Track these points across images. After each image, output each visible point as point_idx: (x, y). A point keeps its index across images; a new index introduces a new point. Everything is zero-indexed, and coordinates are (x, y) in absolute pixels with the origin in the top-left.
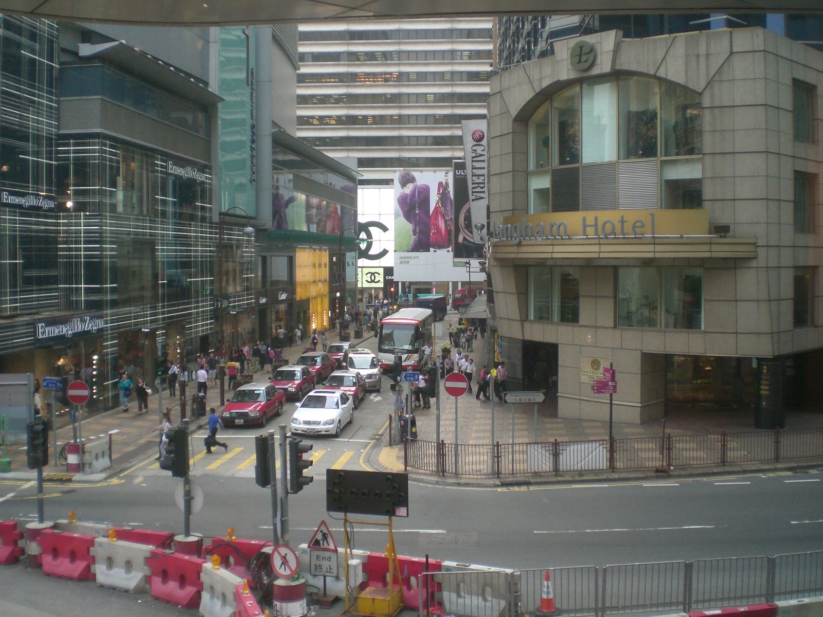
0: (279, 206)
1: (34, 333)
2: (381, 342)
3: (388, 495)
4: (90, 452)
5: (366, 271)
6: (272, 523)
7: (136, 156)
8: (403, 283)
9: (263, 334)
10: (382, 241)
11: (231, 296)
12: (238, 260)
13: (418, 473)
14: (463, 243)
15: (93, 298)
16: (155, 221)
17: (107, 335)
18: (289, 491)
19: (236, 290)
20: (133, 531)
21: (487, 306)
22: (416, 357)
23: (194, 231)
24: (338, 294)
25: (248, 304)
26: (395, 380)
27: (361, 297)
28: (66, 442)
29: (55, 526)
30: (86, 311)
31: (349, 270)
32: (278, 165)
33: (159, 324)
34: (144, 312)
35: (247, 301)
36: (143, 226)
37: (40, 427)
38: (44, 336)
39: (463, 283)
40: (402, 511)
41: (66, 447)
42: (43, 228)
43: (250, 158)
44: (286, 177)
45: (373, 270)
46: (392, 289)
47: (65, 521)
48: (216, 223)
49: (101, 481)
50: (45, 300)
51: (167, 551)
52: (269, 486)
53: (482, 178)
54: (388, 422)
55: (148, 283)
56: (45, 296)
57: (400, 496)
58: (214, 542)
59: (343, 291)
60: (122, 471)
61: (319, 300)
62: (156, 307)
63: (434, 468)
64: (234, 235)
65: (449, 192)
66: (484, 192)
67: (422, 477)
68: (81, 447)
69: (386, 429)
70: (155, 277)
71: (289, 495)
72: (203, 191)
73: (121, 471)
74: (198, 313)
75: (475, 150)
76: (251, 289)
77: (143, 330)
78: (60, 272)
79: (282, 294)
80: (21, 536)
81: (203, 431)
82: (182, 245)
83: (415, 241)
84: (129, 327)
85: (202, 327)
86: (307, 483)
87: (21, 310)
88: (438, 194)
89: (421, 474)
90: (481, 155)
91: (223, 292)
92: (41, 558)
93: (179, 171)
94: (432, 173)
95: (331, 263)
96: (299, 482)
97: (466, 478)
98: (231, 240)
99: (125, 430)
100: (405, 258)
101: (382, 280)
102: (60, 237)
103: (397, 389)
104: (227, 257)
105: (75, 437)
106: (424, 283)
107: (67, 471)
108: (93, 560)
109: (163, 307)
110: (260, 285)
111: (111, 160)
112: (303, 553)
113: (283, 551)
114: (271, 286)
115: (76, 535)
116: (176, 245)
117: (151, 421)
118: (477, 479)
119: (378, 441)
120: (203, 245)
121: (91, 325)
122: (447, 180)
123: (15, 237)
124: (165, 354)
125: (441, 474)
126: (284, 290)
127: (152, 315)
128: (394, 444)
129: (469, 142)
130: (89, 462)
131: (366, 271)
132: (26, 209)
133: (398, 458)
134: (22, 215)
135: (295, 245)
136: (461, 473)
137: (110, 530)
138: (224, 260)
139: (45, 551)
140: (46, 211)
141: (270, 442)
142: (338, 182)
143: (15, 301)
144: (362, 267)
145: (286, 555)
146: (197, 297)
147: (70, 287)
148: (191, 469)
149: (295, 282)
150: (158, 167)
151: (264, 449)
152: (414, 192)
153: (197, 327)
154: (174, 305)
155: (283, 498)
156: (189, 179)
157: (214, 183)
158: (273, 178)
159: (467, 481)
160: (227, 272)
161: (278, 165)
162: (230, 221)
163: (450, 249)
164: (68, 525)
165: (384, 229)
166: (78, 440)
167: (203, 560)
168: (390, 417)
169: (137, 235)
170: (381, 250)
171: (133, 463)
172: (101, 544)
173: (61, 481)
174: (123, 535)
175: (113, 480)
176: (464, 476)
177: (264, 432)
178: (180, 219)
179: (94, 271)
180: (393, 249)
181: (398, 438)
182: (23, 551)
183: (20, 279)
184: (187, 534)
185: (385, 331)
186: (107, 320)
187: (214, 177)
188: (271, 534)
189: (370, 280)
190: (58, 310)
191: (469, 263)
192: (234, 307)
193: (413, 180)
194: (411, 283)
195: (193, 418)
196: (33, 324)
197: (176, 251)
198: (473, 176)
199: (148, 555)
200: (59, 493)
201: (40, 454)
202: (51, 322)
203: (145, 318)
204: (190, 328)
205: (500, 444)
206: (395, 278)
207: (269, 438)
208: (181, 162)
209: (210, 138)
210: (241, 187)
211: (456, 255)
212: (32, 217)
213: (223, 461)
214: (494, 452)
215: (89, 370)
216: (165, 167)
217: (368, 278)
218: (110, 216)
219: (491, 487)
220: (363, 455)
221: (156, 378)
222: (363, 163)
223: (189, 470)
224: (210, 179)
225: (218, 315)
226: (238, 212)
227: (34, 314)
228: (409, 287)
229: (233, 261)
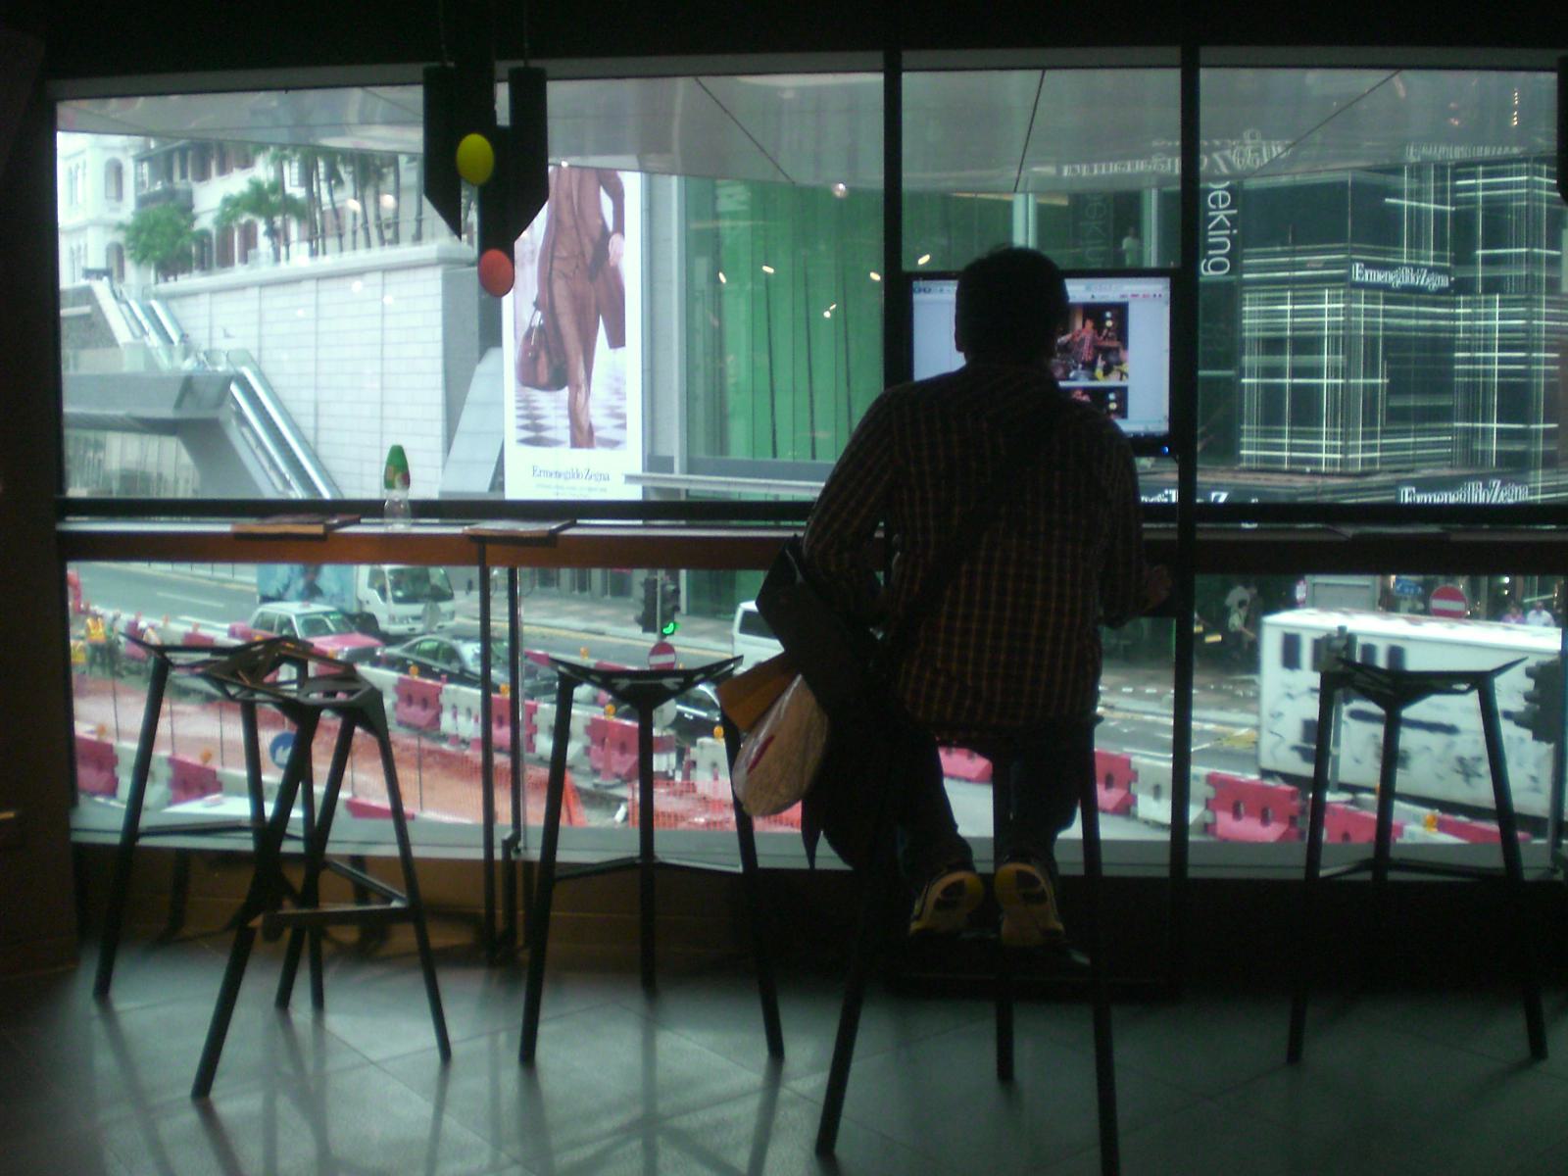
78: (1456, 401)
102: (1459, 339)
132: (1396, 291)
134: (1387, 301)
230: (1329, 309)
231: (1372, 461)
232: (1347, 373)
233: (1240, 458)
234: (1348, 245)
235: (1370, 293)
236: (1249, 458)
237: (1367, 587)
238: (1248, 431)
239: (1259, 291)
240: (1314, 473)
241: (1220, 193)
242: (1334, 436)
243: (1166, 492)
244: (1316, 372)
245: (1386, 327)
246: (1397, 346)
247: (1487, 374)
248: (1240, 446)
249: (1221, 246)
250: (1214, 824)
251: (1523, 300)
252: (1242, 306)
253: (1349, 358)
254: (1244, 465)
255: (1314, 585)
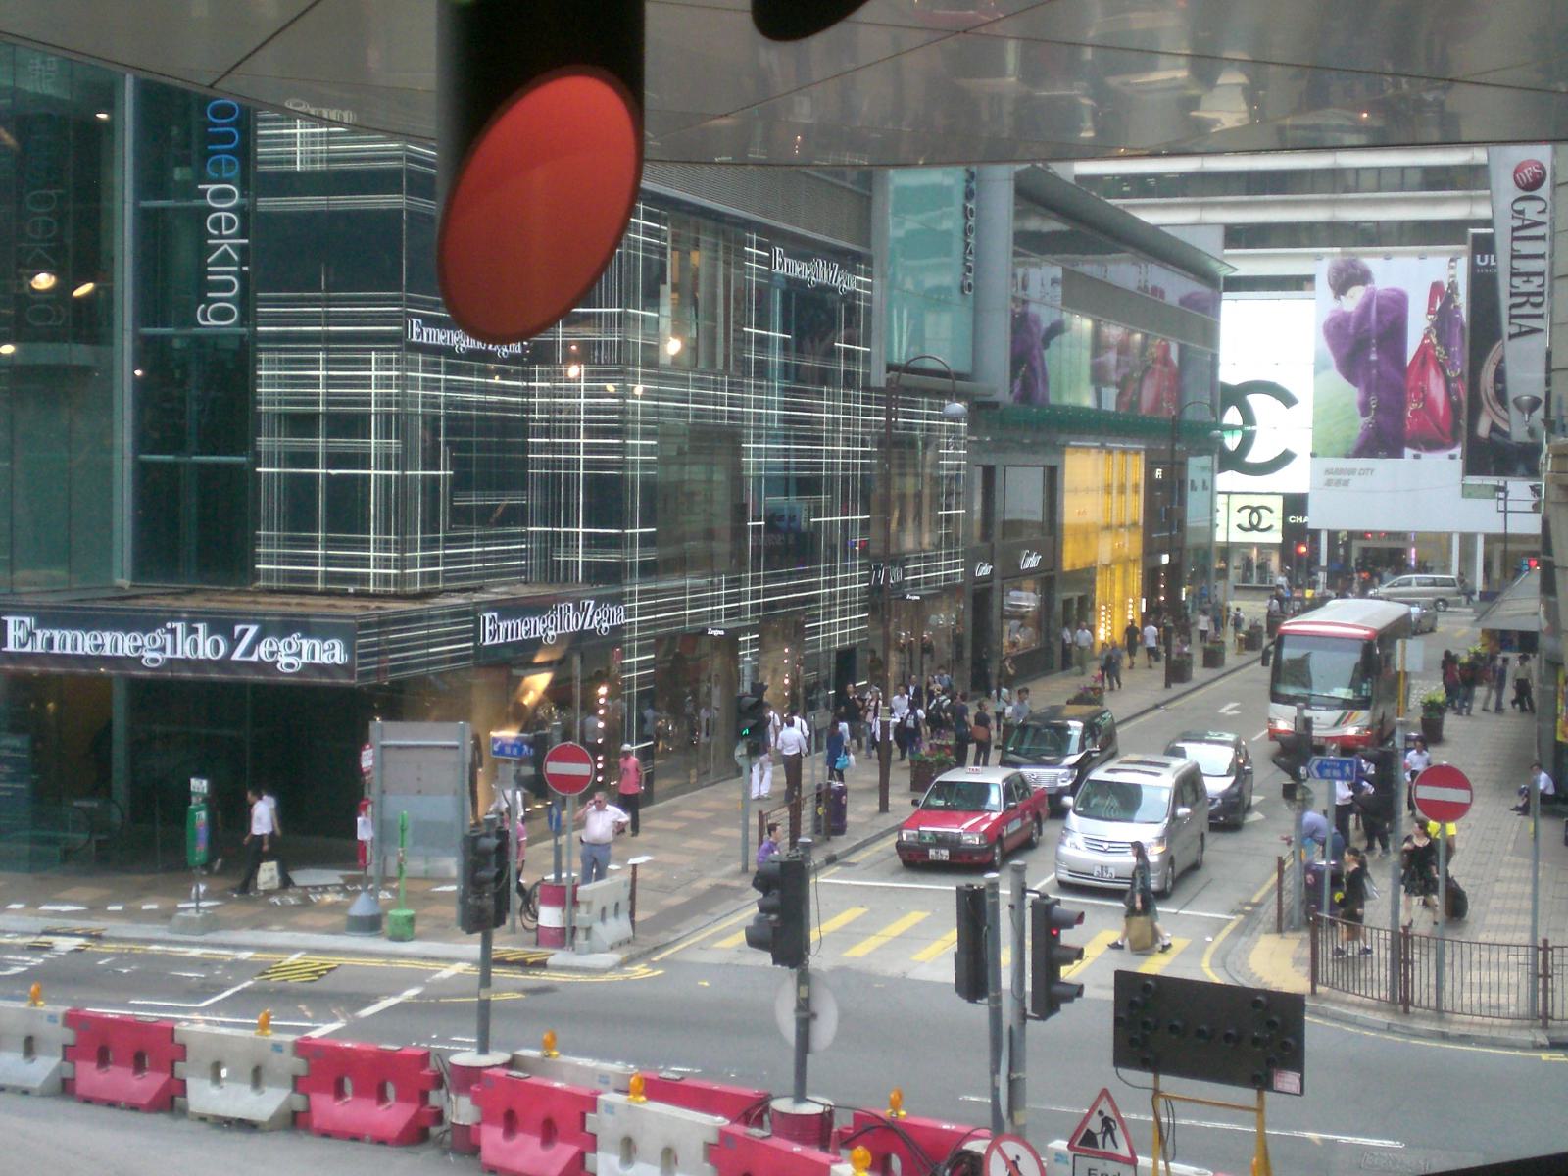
0: (1028, 346)
1: (475, 634)
2: (1277, 678)
3: (1256, 1041)
4: (589, 903)
5: (1238, 501)
6: (989, 1091)
7: (702, 238)
8: (1333, 535)
9: (971, 675)
10: (1276, 429)
11: (908, 559)
12: (928, 471)
13: (1342, 1002)
14: (1490, 438)
15: (599, 558)
16: (741, 385)
17: (631, 640)
18: (1029, 1012)
19: (921, 544)
20: (682, 1082)
21: (1542, 601)
22: (1363, 716)
23: (828, 408)
24: (1165, 559)
25: (947, 578)
26: (1295, 775)
27: (1223, 565)
28: (538, 878)
29: (510, 1064)
30: (587, 587)
31: (1194, 501)
32: (1029, 244)
33: (746, 620)
34: (714, 590)
35: (949, 570)
36: (716, 396)
37: (492, 842)
38: (495, 641)
39: (1489, 539)
40: (1288, 1080)
41: (538, 890)
42: (494, 398)
43: (961, 235)
44: (1044, 275)
45: (1255, 501)
46: (1303, 549)
47: (533, 1053)
48: (879, 390)
49: (611, 969)
50: (497, 560)
51: (755, 1132)
52: (985, 1000)
53: (1537, 281)
54: (1275, 876)
55: (723, 524)
56: (496, 552)
57: (1285, 1045)
58: (857, 1118)
59: (1176, 548)
60: (657, 949)
61: (1119, 572)
62: (739, 580)
63: (1382, 993)
64: (920, 416)
65: (1457, 307)
66: (1540, 316)
67: (1344, 1011)
68: (569, 891)
69: (1270, 892)
70: (740, 511)
71: (1028, 1021)
72: (852, 310)
73: (655, 948)
74: (832, 596)
75: (1521, 212)
76: (957, 544)
77: (710, 632)
78: (531, 499)
79: (1028, 555)
80: (438, 1082)
81: (838, 868)
82: (799, 439)
83: (1366, 430)
84: (678, 624)
85: (840, 628)
86: (1069, 998)
87: (447, 580)
88: (1429, 313)
89: (1352, 1004)
90: (1536, 224)
91: (893, 550)
92: (478, 1132)
93: (802, 270)
94: (1414, 260)
95: (1151, 484)
96: (1051, 995)
97: (1462, 1023)
98: (912, 429)
99: (667, 857)
100: (1340, 472)
101: (1278, 525)
102: (533, 420)
103: (1298, 796)
104: (901, 466)
105: (558, 870)
106: (1390, 535)
107: (537, 943)
108: (592, 1143)
109: (755, 581)
110: (977, 530)
111: (647, 247)
112: (1057, 1161)
113: (1012, 1148)
114: (1004, 535)
115: (557, 1085)
116: (787, 439)
117: (723, 838)
118: (1491, 1026)
119: (1249, 919)
120: (847, 439)
121: (599, 619)
122: (1453, 276)
123: (436, 418)
124: (758, 689)
125: (1401, 1008)
126: (1034, 547)
127: (730, 598)
128: (1288, 929)
129: (1505, 188)
130: (588, 925)
131: (1238, 501)
132: (459, 356)
133: (1297, 961)
134: (452, 369)
135: (1062, 439)
136: (1449, 1008)
137: (632, 1076)
138: (894, 471)
139: (487, 1117)
140: (504, 361)
141: (989, 900)
142: (1175, 287)
143: (433, 561)
144: (1229, 493)
145: (1018, 1157)
146: (832, 559)
147: (552, 532)
148: (813, 950)
149: (1062, 525)
150: (751, 261)
151: (975, 916)
152: (1366, 307)
153: (829, 628)
154: (779, 578)
155: (1015, 1028)
156: (823, 289)
157: (877, 294)
158: (1015, 276)
159: (1464, 1030)
160: (902, 497)
161: (1029, 244)
162: (915, 381)
163: (1458, 451)
164: (543, 1061)
165: (1288, 400)
166: (564, 875)
167: (832, 1157)
168: (1281, 862)
169: (701, 417)
170: (1277, 453)
171: (680, 935)
172: (611, 1108)
173: (522, 965)
174: (659, 1090)
175: (636, 968)
176: (1457, 1018)
177: (979, 882)
178: (798, 380)
179: (607, 498)
180: (1310, 450)
181: (1298, 914)
182: (439, 1117)
183: (444, 512)
184: (800, 1097)
185: (1288, 653)
186: (632, 608)
187: (877, 282)
188: (987, 1116)
189: (1247, 525)
190: (526, 583)
191: (1503, 489)
192: (916, 583)
193: (1364, 278)
194: (1352, 535)
195: (819, 837)
196: (472, 614)
197: (786, 453)
198: (1513, 275)
199: (714, 1138)
200: (519, 992)
201: (488, 902)
202: (510, 609)
203: (713, 603)
204: (815, 631)
205: (1550, 945)
206: (1312, 520)
207: (988, 891)
208: (803, 249)
209: (871, 190)
210: (936, 299)
211: (1473, 467)
212: (472, 376)
213: (883, 940)
214: (1535, 965)
215: (590, 720)
216: (768, 262)
217: (1243, 518)
218: (643, 375)
219: (1523, 1048)
220: (1211, 949)
221: (737, 744)
222: (1238, 236)
223: (809, 953)
224: (869, 287)
225: (879, 602)
226: (929, 364)
227: (475, 590)
228: (1347, 546)
229: (917, 475)
230: (378, 378)
231: (434, 577)
232: (402, 465)
233: (256, 576)
234: (403, 294)
235: (431, 358)
236: (269, 575)
237: (456, 747)
238: (267, 538)
239: (281, 350)
240: (357, 595)
241: (224, 214)
242: (386, 545)
243: (169, 625)
244: (363, 460)
245: (450, 404)
246: (459, 425)
247: (571, 464)
248: (255, 559)
249: (227, 286)
250: (308, 1111)
251: (616, 373)
252: (256, 369)
253: (404, 443)
254: (261, 584)
255: (384, 747)
